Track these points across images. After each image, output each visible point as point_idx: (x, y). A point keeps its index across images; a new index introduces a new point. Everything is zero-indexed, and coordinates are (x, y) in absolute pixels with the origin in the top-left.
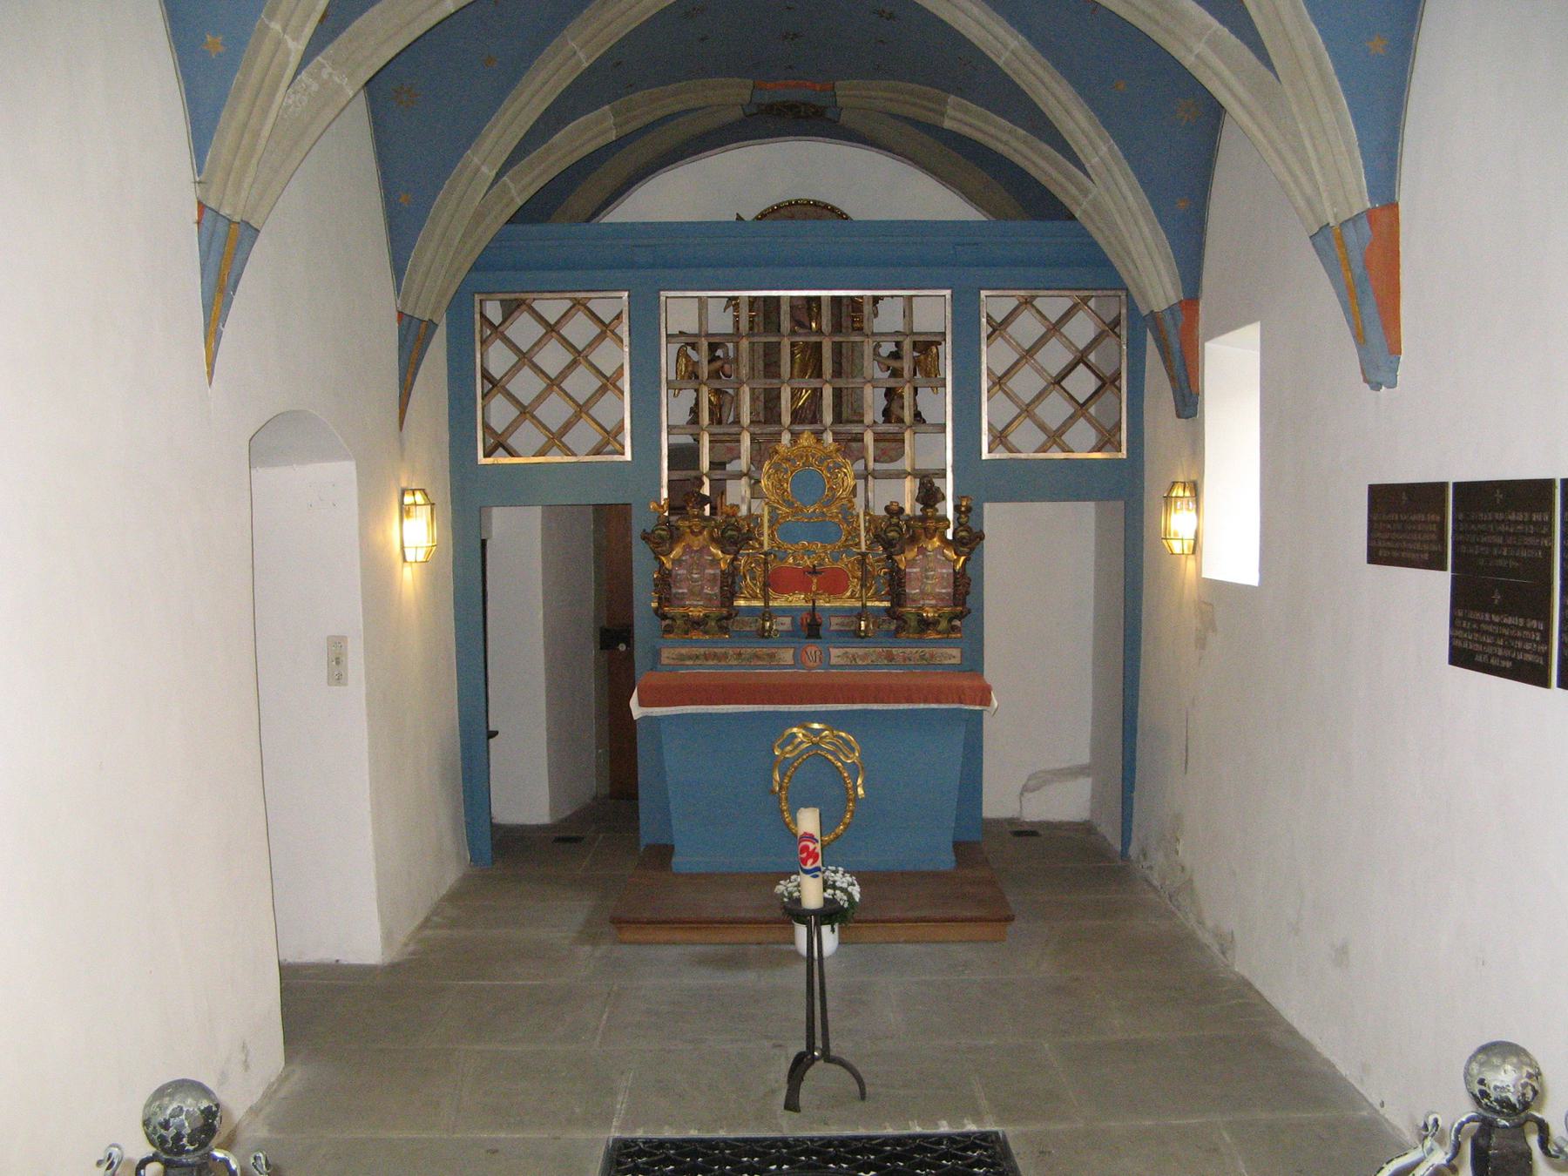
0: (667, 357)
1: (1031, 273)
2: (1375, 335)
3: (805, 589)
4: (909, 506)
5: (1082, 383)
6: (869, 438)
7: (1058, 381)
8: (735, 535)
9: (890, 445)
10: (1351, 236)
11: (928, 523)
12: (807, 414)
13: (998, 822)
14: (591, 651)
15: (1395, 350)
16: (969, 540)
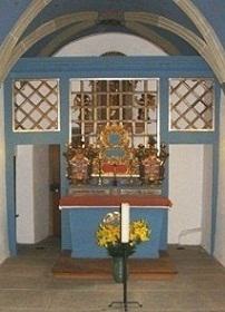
0: (72, 98)
1: (184, 74)
3: (113, 171)
4: (147, 146)
5: (200, 107)
6: (134, 124)
7: (193, 106)
8: (92, 154)
9: (141, 127)
11: (152, 151)
12: (116, 117)
13: (172, 245)
14: (48, 189)
16: (165, 156)
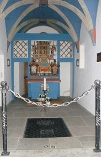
1: (64, 40)
2: (94, 41)
5: (69, 50)
7: (67, 50)
10: (92, 31)
14: (23, 79)
15: (95, 42)
16: (59, 66)
